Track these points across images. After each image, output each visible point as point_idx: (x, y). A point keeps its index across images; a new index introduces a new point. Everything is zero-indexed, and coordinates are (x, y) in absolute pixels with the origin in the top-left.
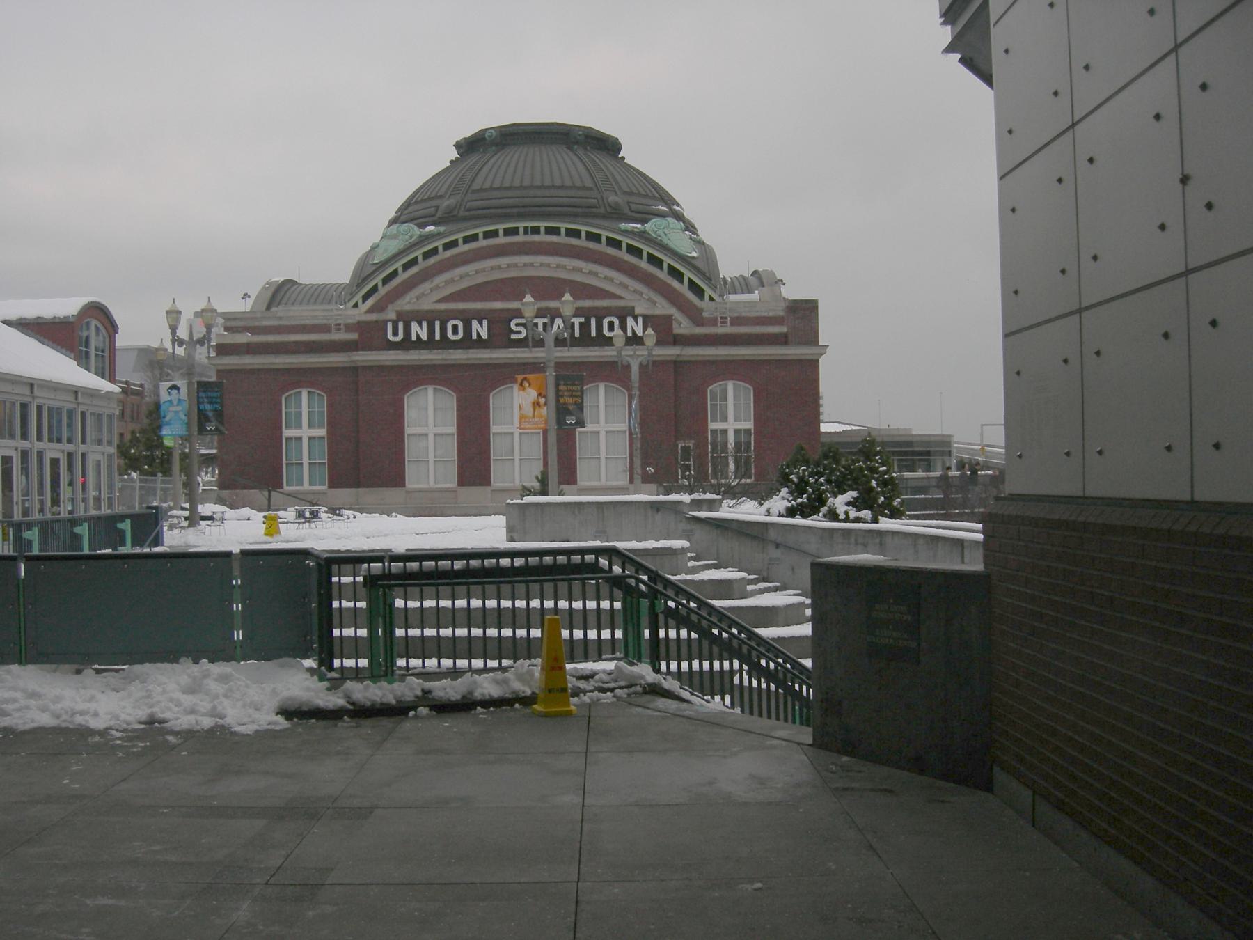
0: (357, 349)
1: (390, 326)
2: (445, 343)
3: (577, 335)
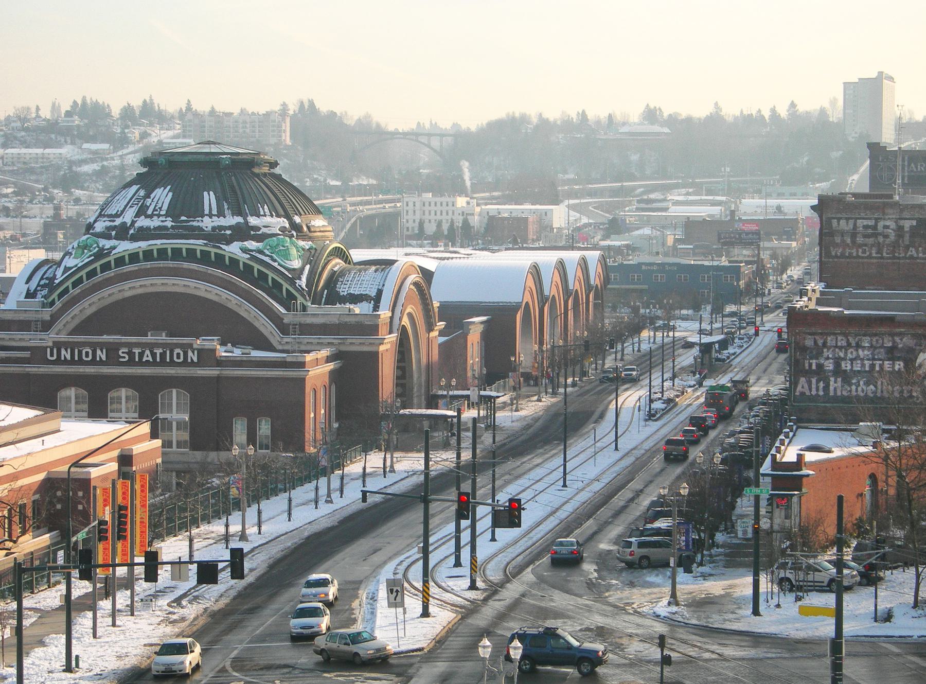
0: (135, 343)
1: (49, 350)
2: (81, 362)
3: (158, 360)
